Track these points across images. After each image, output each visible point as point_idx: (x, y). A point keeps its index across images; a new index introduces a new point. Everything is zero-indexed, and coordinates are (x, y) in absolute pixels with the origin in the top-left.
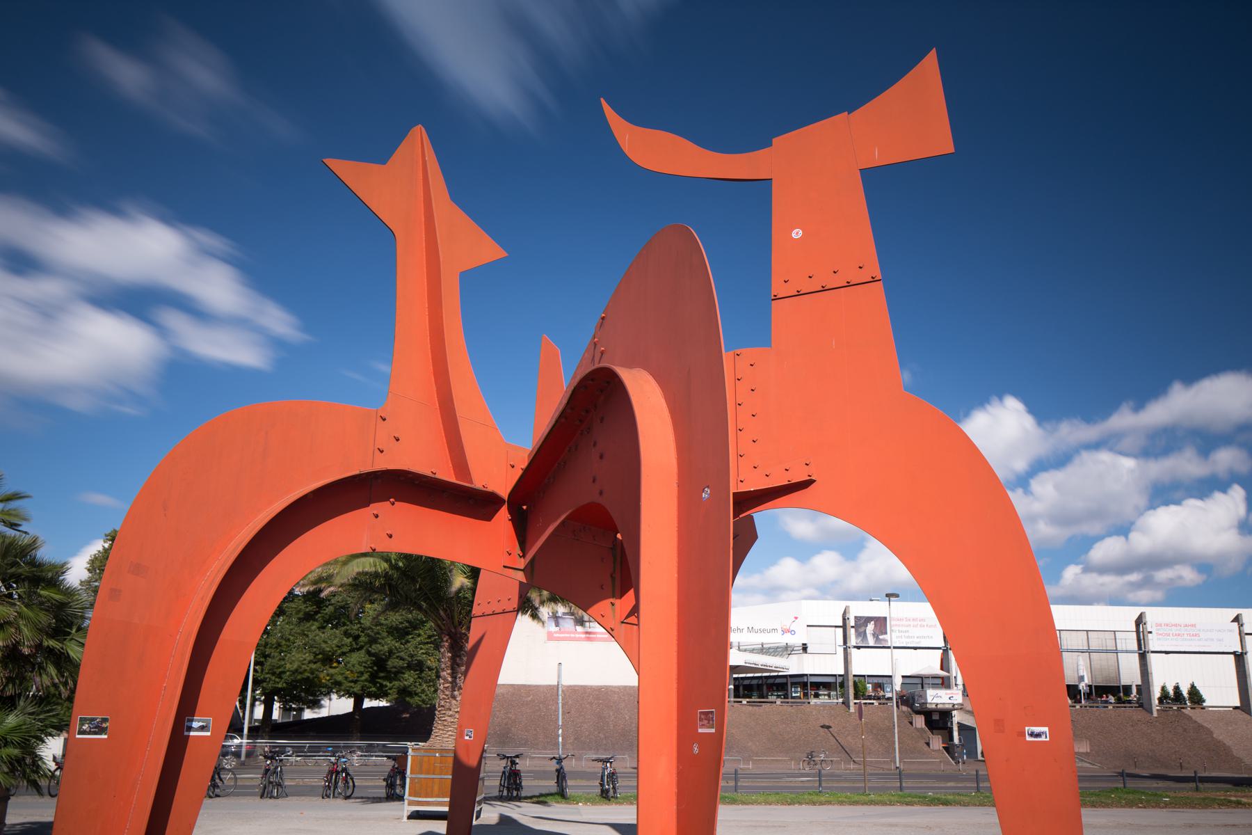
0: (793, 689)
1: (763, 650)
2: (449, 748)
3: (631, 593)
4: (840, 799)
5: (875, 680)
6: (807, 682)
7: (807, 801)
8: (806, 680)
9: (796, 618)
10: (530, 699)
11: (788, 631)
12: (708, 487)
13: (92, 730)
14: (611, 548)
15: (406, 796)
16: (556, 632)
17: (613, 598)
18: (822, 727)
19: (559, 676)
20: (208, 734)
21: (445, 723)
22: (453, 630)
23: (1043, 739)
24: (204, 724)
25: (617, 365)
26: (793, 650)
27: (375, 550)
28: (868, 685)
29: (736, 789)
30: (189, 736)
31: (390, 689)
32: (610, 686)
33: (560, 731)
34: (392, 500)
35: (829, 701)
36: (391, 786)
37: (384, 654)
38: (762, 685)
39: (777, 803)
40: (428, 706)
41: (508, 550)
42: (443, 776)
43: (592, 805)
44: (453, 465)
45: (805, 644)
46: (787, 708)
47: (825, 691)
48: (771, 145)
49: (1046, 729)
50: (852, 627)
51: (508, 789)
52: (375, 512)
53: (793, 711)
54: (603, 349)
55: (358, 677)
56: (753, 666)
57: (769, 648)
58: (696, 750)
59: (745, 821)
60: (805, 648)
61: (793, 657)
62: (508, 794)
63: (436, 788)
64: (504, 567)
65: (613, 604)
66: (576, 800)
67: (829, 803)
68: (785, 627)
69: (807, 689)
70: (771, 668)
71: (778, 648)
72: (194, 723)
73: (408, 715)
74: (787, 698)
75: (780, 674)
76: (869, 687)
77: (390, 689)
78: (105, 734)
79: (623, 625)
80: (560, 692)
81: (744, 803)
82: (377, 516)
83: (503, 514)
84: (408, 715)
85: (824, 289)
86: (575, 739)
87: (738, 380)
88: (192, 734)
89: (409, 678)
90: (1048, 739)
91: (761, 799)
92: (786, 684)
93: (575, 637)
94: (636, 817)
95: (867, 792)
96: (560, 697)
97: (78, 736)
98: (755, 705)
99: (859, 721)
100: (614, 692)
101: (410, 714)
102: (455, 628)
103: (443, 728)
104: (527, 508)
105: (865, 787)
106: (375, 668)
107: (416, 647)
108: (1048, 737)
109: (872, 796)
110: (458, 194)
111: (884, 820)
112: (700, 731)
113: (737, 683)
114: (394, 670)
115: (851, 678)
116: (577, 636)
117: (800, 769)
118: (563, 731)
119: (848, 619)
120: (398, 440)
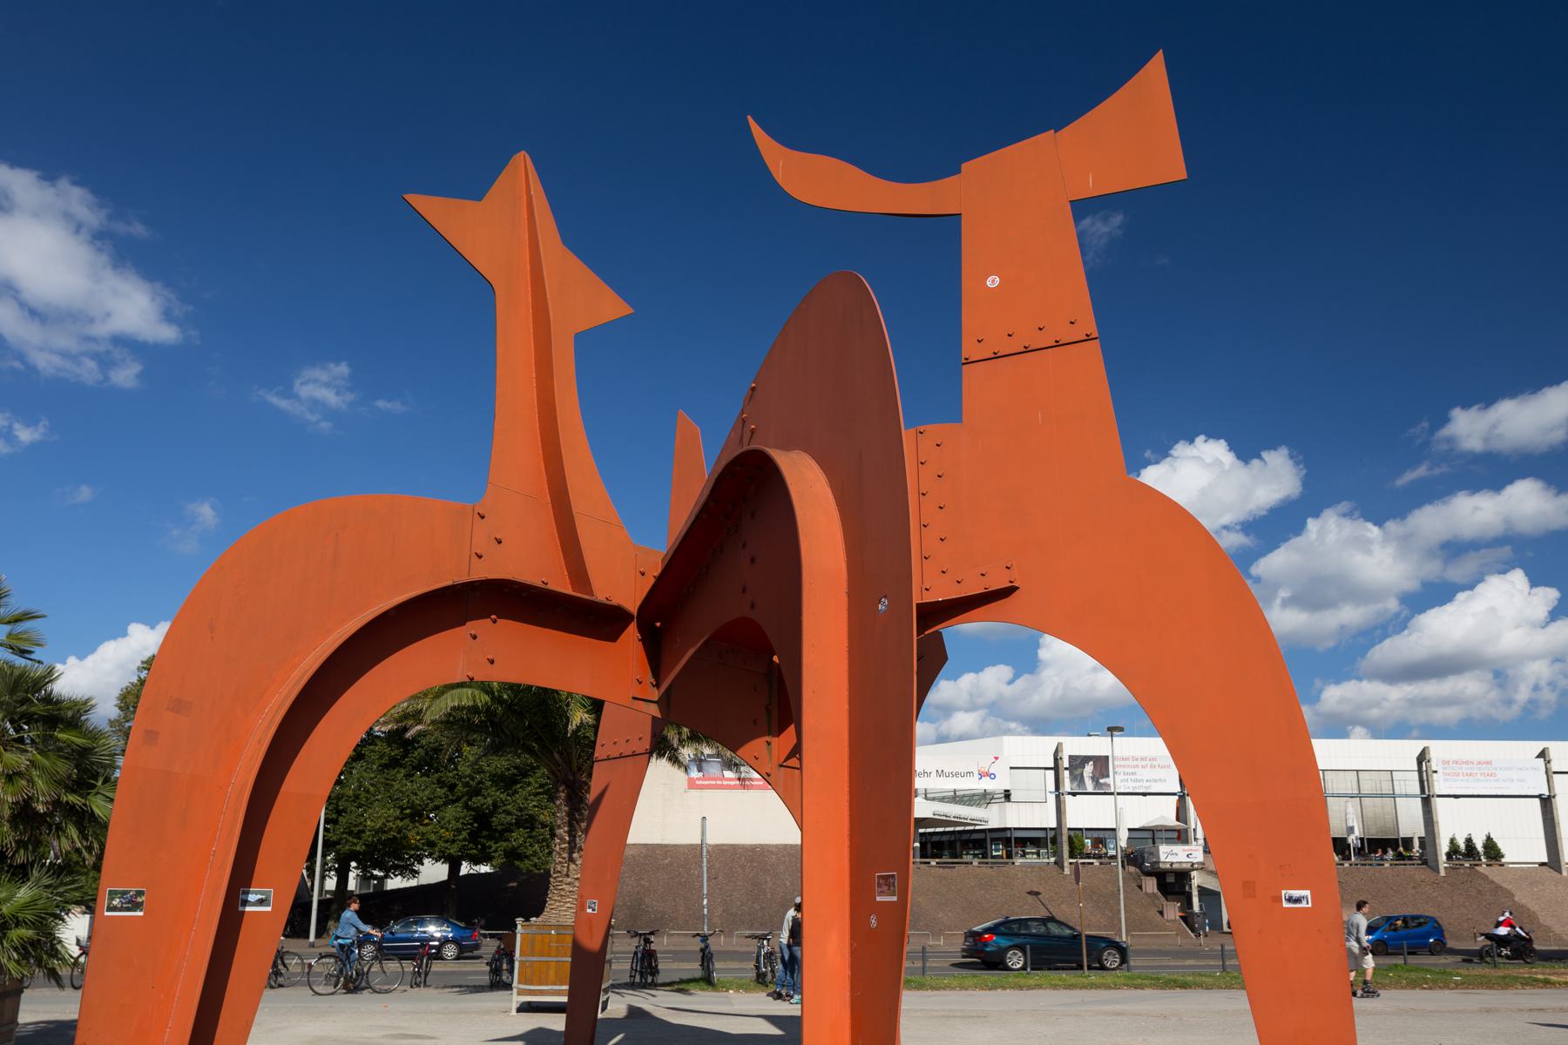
0: (993, 847)
1: (956, 798)
2: (568, 924)
3: (792, 729)
5: (1096, 835)
6: (1010, 838)
7: (1012, 985)
8: (1009, 835)
9: (996, 758)
10: (667, 861)
12: (885, 597)
13: (124, 905)
15: (515, 984)
16: (698, 779)
17: (769, 735)
18: (1029, 893)
19: (703, 833)
20: (269, 909)
21: (563, 893)
22: (571, 778)
23: (1303, 905)
24: (263, 897)
26: (993, 798)
28: (1086, 841)
30: (243, 912)
31: (496, 851)
34: (493, 617)
39: (976, 987)
42: (560, 959)
45: (1008, 791)
46: (986, 870)
49: (1307, 893)
50: (1066, 769)
52: (473, 632)
53: (994, 873)
54: (753, 427)
56: (944, 818)
57: (964, 796)
58: (874, 922)
60: (1007, 795)
61: (994, 808)
62: (641, 980)
63: (552, 973)
65: (769, 743)
68: (983, 770)
69: (1011, 847)
70: (965, 821)
71: (974, 795)
72: (250, 895)
73: (515, 884)
74: (987, 858)
75: (977, 828)
76: (1088, 842)
77: (496, 851)
78: (141, 910)
80: (705, 853)
81: (933, 988)
82: (475, 637)
83: (632, 633)
84: (515, 884)
85: (1027, 350)
86: (724, 911)
87: (922, 463)
88: (248, 909)
89: (518, 837)
90: (1310, 905)
92: (985, 840)
97: (107, 914)
98: (947, 867)
100: (772, 853)
102: (574, 775)
103: (559, 898)
110: (572, 238)
112: (879, 899)
113: (924, 840)
115: (1065, 832)
116: (725, 783)
119: (1061, 758)
120: (500, 542)
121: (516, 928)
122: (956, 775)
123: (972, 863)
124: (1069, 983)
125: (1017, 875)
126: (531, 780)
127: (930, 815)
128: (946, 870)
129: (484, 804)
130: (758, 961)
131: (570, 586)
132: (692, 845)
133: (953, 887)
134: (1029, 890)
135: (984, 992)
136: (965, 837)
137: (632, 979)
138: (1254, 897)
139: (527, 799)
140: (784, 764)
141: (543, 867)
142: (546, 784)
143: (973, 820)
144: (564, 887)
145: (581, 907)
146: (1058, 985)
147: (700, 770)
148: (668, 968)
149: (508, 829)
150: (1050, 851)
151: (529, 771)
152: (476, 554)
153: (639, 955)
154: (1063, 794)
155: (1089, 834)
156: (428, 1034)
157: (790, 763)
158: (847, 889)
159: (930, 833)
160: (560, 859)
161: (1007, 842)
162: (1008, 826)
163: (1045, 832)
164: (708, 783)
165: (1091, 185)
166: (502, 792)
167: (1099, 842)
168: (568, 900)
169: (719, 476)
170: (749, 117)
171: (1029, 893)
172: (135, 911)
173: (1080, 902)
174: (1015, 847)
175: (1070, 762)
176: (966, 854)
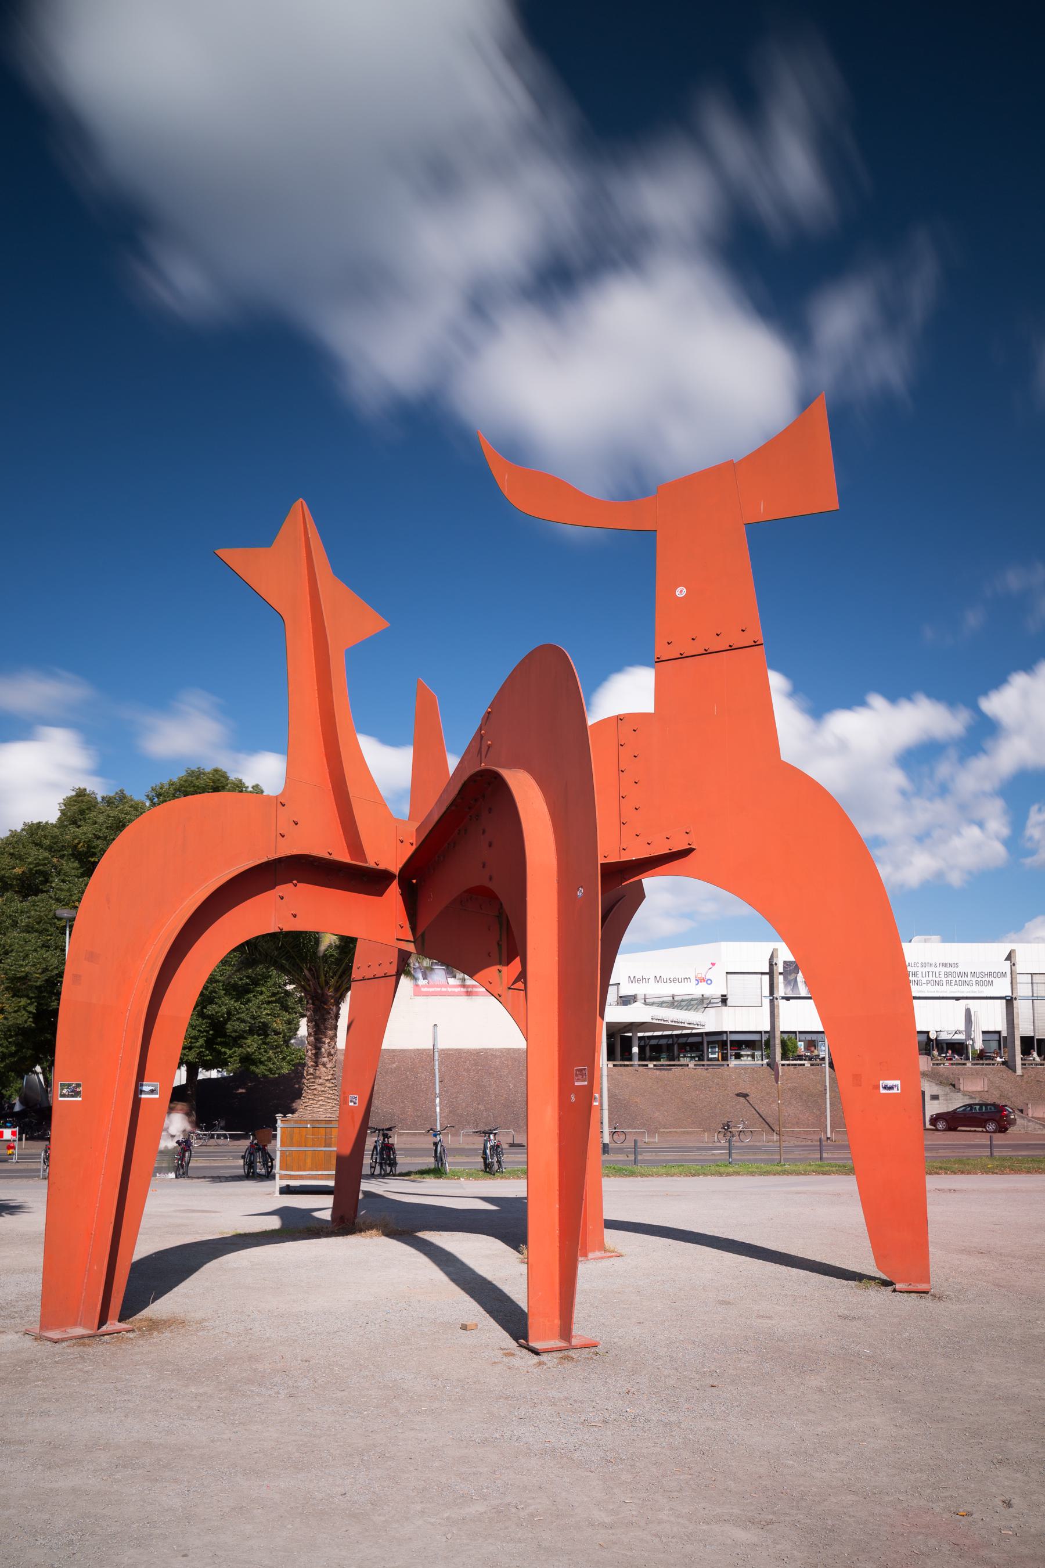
1: (674, 1003)
2: (321, 1119)
3: (517, 961)
4: (750, 1170)
5: (809, 1037)
6: (726, 1041)
7: (713, 1172)
8: (725, 1039)
9: (713, 964)
11: (704, 980)
12: (582, 887)
13: (70, 1094)
14: (498, 916)
15: (277, 1170)
16: (424, 986)
17: (500, 964)
18: (738, 1095)
19: (435, 1039)
20: (157, 1096)
21: (315, 1092)
22: (319, 991)
23: (895, 1091)
24: (153, 1088)
25: (504, 767)
28: (799, 1043)
29: (635, 1162)
31: (231, 1057)
32: (490, 1049)
33: (438, 1100)
34: (295, 882)
35: (753, 1063)
38: (672, 1045)
39: (680, 1174)
40: (277, 1075)
41: (400, 923)
42: (316, 1149)
43: (475, 1179)
44: (347, 844)
45: (725, 996)
46: (701, 1071)
47: (748, 1051)
49: (898, 1082)
50: (781, 974)
53: (708, 1075)
54: (489, 742)
55: (191, 1042)
56: (662, 1022)
57: (682, 1001)
58: (573, 1099)
60: (724, 1000)
61: (711, 1012)
62: (381, 1171)
63: (309, 1161)
64: (398, 939)
65: (500, 971)
66: (456, 1176)
67: (737, 1173)
68: (700, 976)
69: (727, 1049)
70: (683, 1025)
71: (692, 1000)
73: (244, 1091)
74: (703, 1060)
75: (694, 1031)
76: (801, 1045)
77: (231, 1057)
78: (80, 1097)
79: (510, 990)
80: (436, 1057)
81: (642, 1175)
82: (282, 898)
83: (394, 889)
84: (244, 1091)
85: (707, 653)
86: (450, 1112)
87: (621, 745)
88: (143, 1096)
89: (252, 1044)
90: (899, 1091)
91: (662, 1170)
92: (702, 1043)
93: (447, 992)
94: (526, 1189)
95: (782, 1163)
98: (664, 1069)
99: (774, 1083)
100: (495, 1057)
101: (247, 1089)
102: (322, 989)
103: (313, 1097)
105: (780, 1158)
108: (899, 1089)
110: (339, 571)
111: (794, 1189)
112: (576, 1084)
113: (642, 1043)
114: (234, 1034)
115: (778, 1034)
116: (450, 990)
118: (440, 1099)
119: (776, 964)
120: (296, 824)
121: (276, 1123)
123: (688, 1065)
126: (263, 989)
127: (649, 1020)
128: (663, 1072)
129: (219, 1012)
130: (485, 1153)
133: (669, 1089)
134: (736, 1093)
136: (682, 1040)
137: (373, 1169)
138: (860, 1086)
139: (259, 1007)
140: (512, 987)
141: (278, 1072)
142: (278, 993)
143: (690, 1024)
144: (316, 1087)
145: (344, 1101)
146: (753, 1172)
148: (403, 1162)
149: (242, 1037)
150: (764, 1053)
151: (261, 980)
154: (777, 999)
155: (803, 1037)
157: (516, 986)
159: (677, 1035)
161: (723, 1045)
162: (725, 1029)
164: (431, 990)
166: (235, 1001)
167: (811, 1045)
168: (320, 1098)
169: (465, 782)
171: (738, 1095)
174: (731, 1050)
175: (784, 967)
176: (684, 1057)
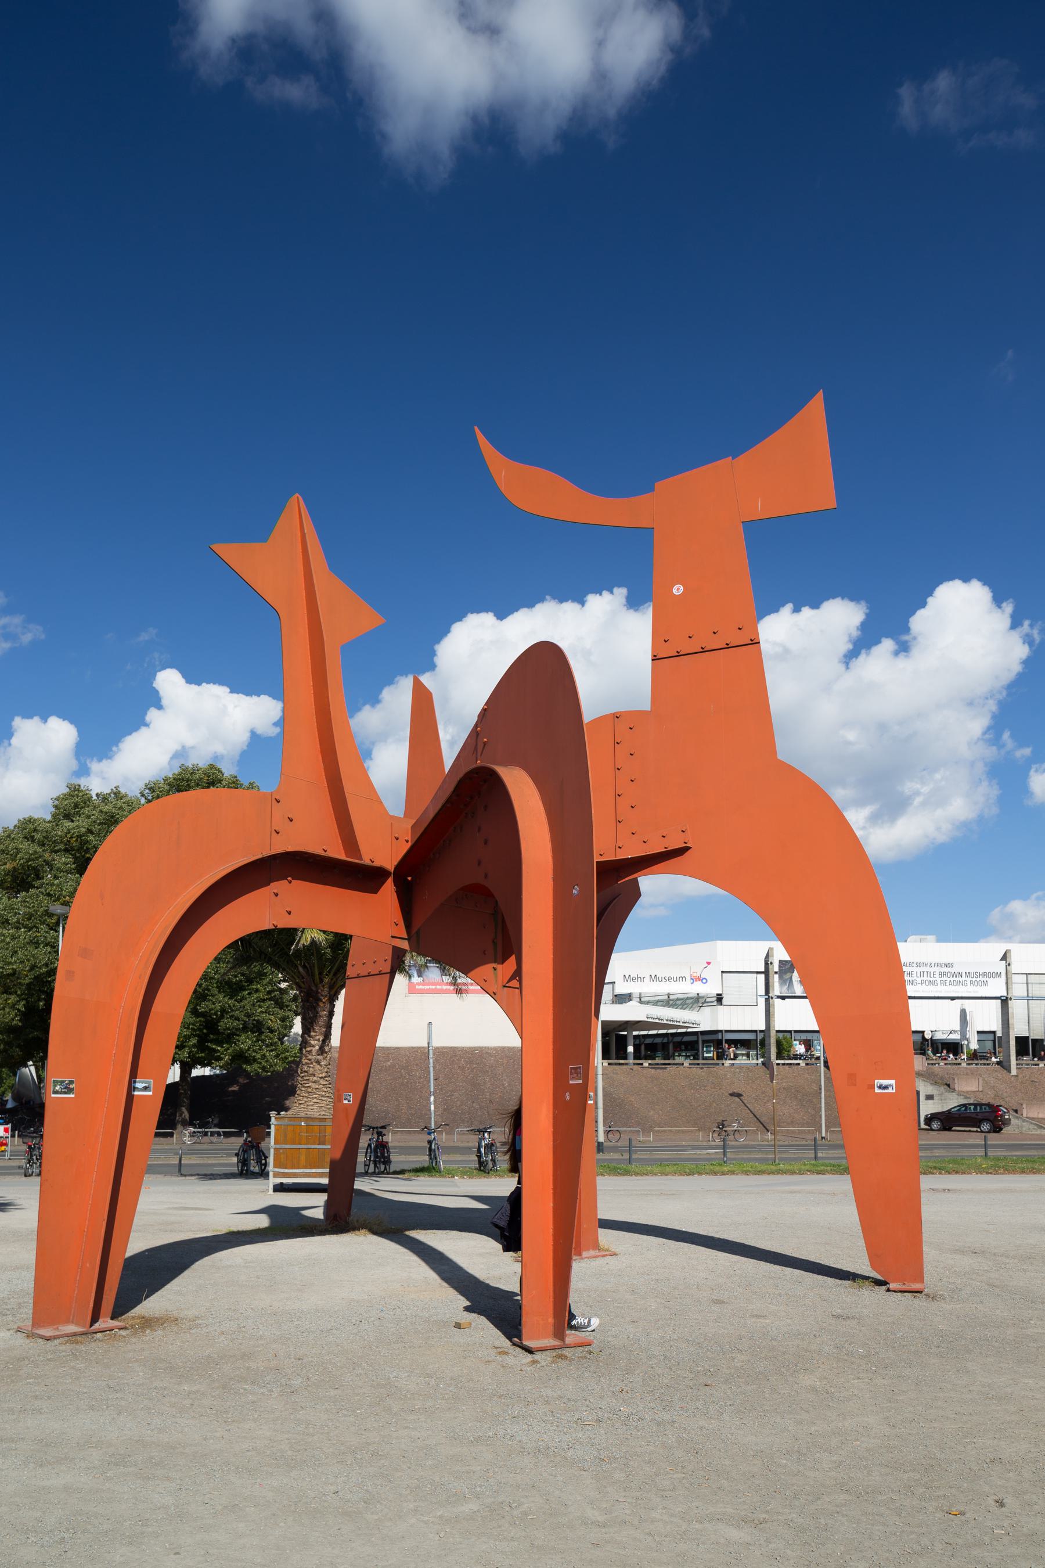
0: (705, 1049)
1: (669, 1002)
2: (315, 1116)
3: (513, 959)
4: (745, 1169)
5: (804, 1036)
7: (708, 1171)
8: (720, 1038)
9: (709, 963)
10: (389, 1063)
12: (577, 885)
13: (63, 1090)
14: (493, 914)
15: (271, 1167)
16: (419, 984)
18: (732, 1095)
19: (429, 1037)
20: (150, 1093)
21: (310, 1090)
22: (314, 988)
23: (890, 1091)
24: (147, 1085)
26: (705, 1002)
27: (277, 926)
28: (794, 1042)
29: (630, 1161)
30: (134, 1095)
33: (432, 1098)
34: (289, 878)
36: (244, 1162)
37: (216, 1014)
38: (668, 1043)
39: (675, 1173)
40: (270, 1074)
41: (395, 921)
42: (310, 1146)
45: (720, 995)
46: (696, 1071)
48: (654, 491)
49: (893, 1082)
50: (776, 973)
51: (375, 1162)
52: (276, 891)
53: (703, 1074)
54: (485, 740)
56: (657, 1021)
57: (678, 999)
58: (568, 1097)
59: (636, 1190)
60: (719, 999)
61: (706, 1011)
62: (375, 1169)
63: (303, 1158)
64: (393, 937)
65: (495, 969)
66: (451, 1174)
67: (732, 1173)
68: (695, 975)
70: (678, 1024)
71: (687, 998)
72: (136, 1084)
74: (698, 1059)
75: (689, 1030)
78: (73, 1094)
80: (431, 1055)
81: (637, 1174)
82: (277, 895)
83: (389, 887)
85: (703, 651)
86: (445, 1110)
87: (618, 743)
88: (136, 1093)
89: (245, 1042)
90: (894, 1091)
91: (656, 1169)
92: (697, 1042)
95: (777, 1161)
96: (431, 1061)
97: (53, 1096)
98: (658, 1068)
99: (769, 1082)
100: (490, 1055)
102: (316, 986)
103: (307, 1095)
104: (412, 879)
105: (775, 1158)
106: (205, 1031)
107: (254, 1005)
109: (781, 1165)
110: (335, 564)
112: (571, 1082)
113: (637, 1042)
115: (773, 1034)
117: (709, 1141)
119: (771, 963)
120: (291, 820)
121: (270, 1121)
122: (669, 979)
123: (683, 1064)
124: (759, 1169)
125: (725, 1075)
128: (658, 1070)
131: (343, 852)
132: (413, 1048)
133: (664, 1087)
134: (731, 1092)
135: (683, 1177)
136: (677, 1039)
137: (367, 1167)
138: (855, 1085)
140: (507, 985)
143: (685, 1023)
144: (310, 1084)
147: (419, 976)
148: (397, 1160)
152: (275, 830)
153: (373, 1146)
154: (772, 998)
155: (798, 1036)
156: (204, 1207)
158: (551, 1076)
159: (672, 1034)
160: (307, 1061)
161: (718, 1044)
163: (755, 1034)
165: (759, 509)
168: (314, 1096)
170: (476, 428)
172: (69, 1094)
173: (773, 1099)
175: (780, 966)
176: (679, 1056)
